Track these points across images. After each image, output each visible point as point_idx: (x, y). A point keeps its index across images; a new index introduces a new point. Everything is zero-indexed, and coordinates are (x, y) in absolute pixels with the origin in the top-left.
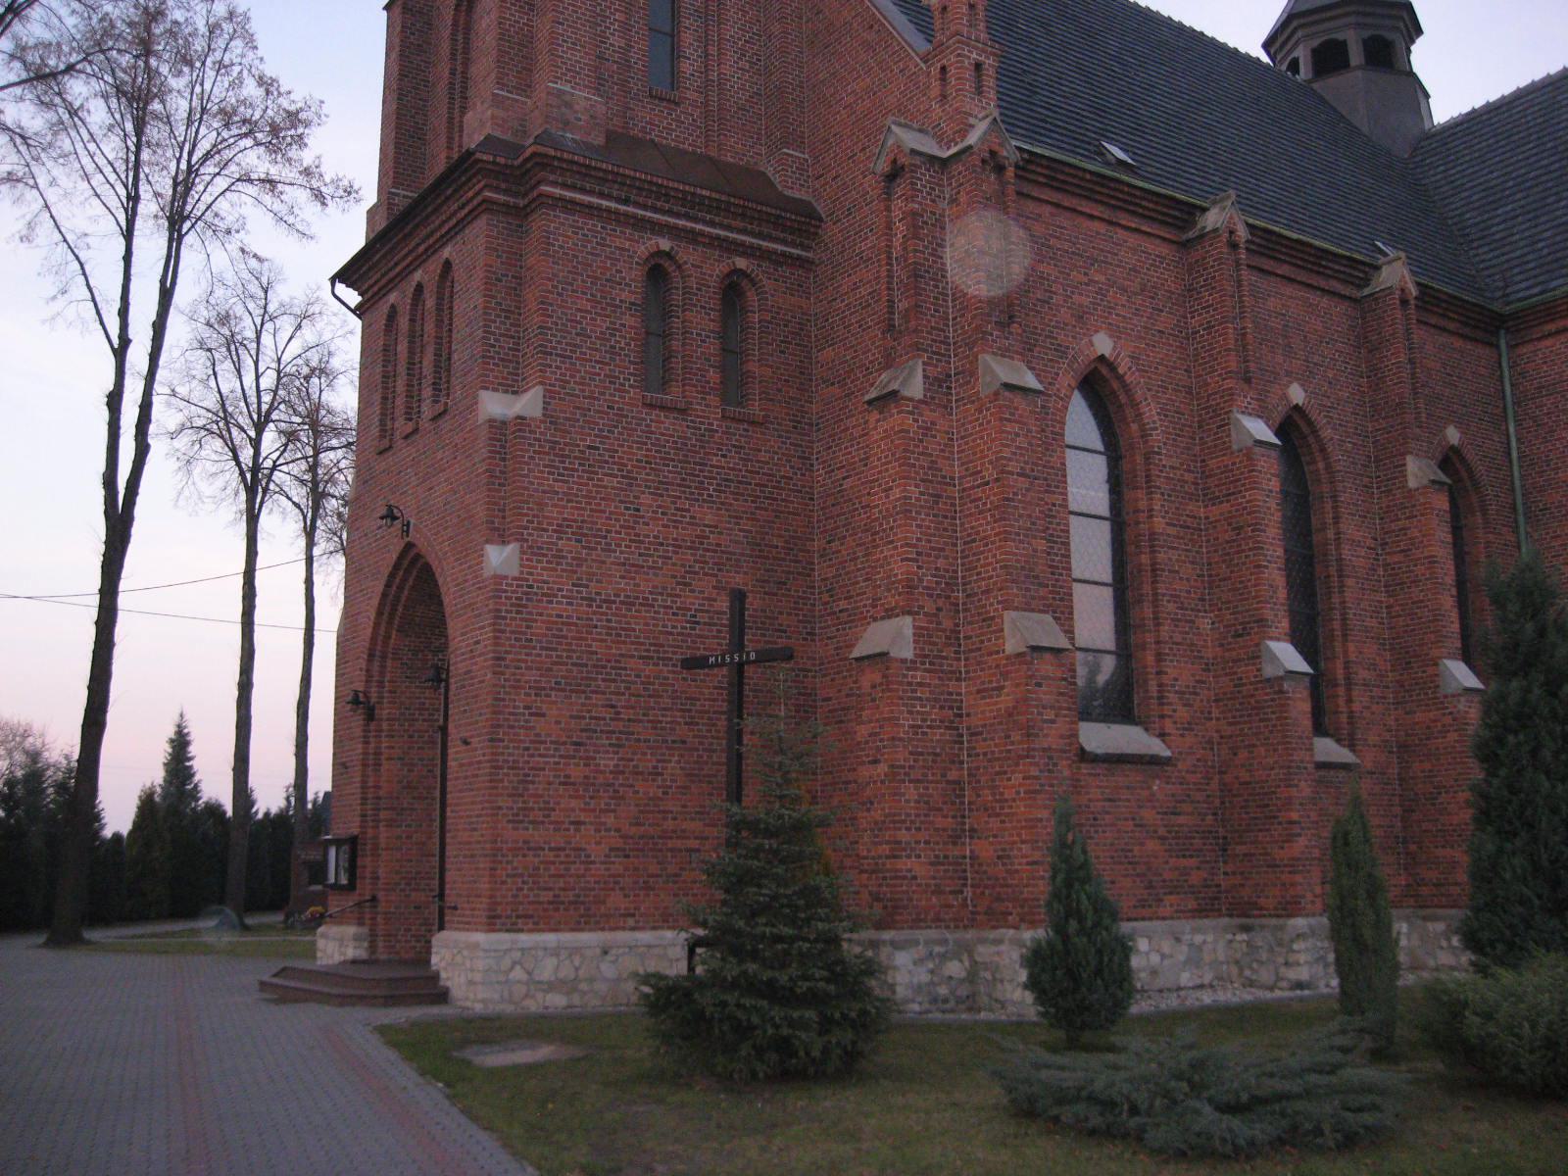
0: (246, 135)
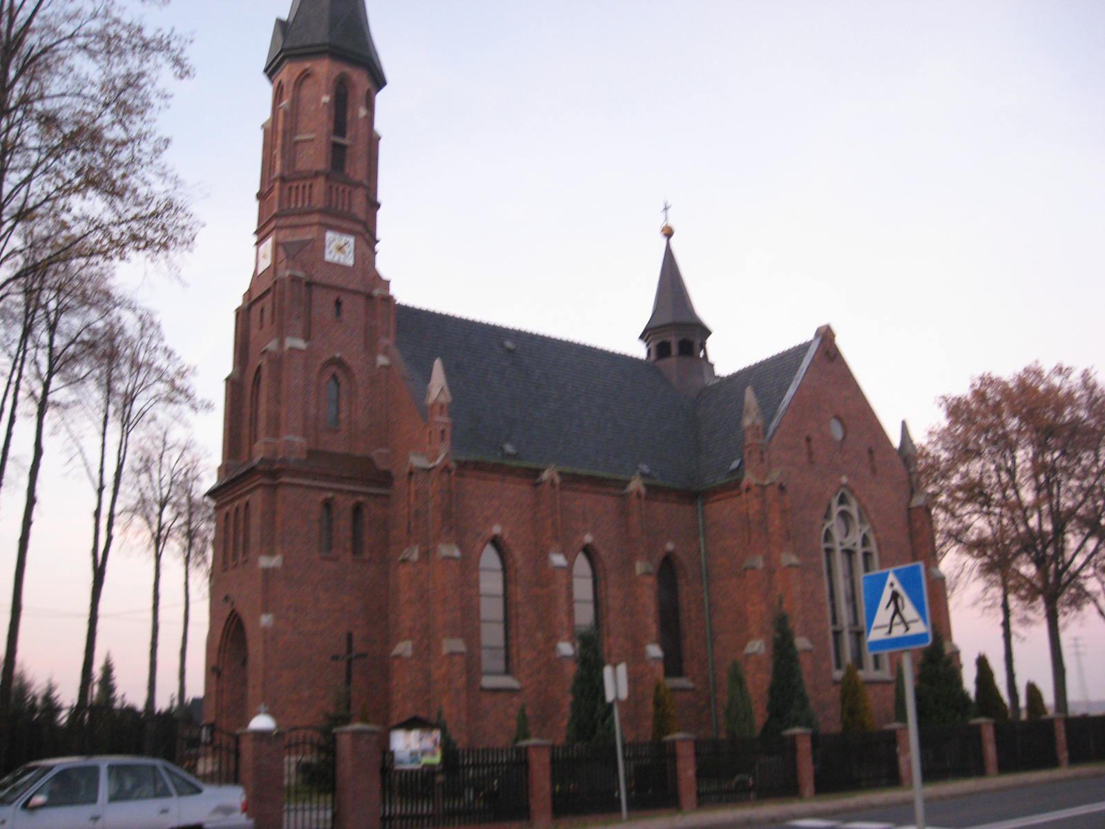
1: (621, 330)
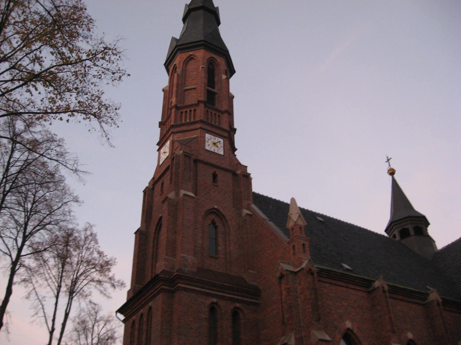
0: (93, 268)
1: (376, 220)
